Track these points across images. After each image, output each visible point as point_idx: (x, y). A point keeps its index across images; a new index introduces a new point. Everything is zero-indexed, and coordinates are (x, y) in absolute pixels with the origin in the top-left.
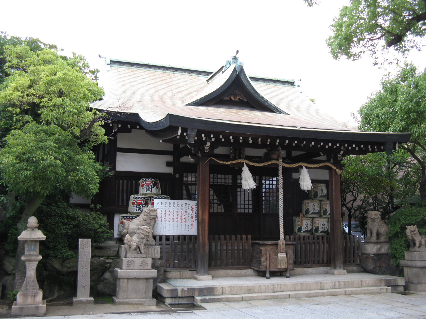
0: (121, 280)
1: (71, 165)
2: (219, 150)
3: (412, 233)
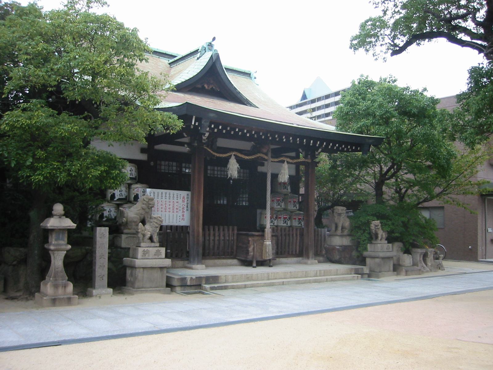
0: (138, 270)
3: (376, 227)
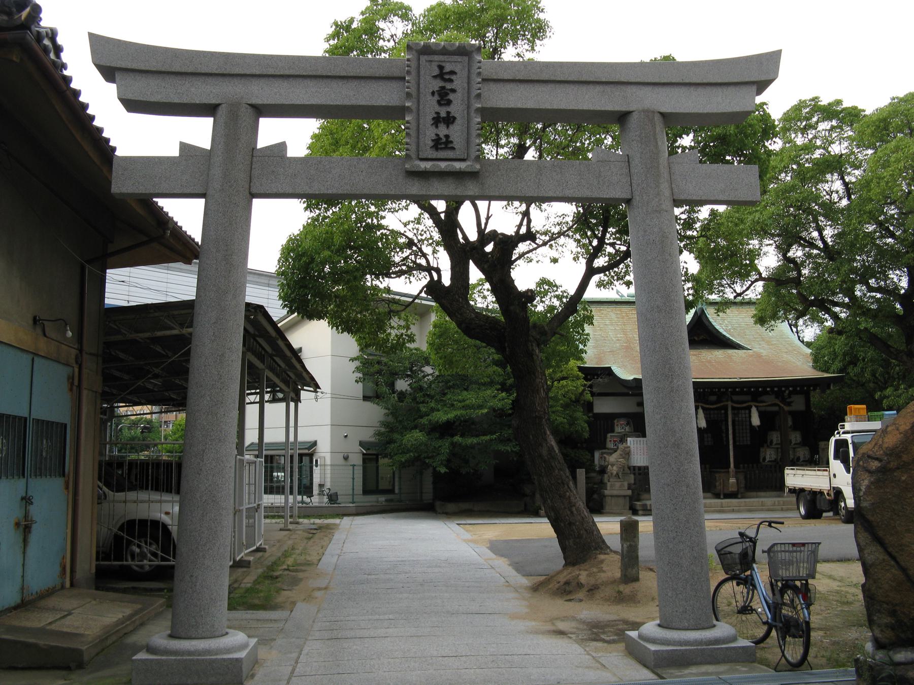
1: (572, 421)
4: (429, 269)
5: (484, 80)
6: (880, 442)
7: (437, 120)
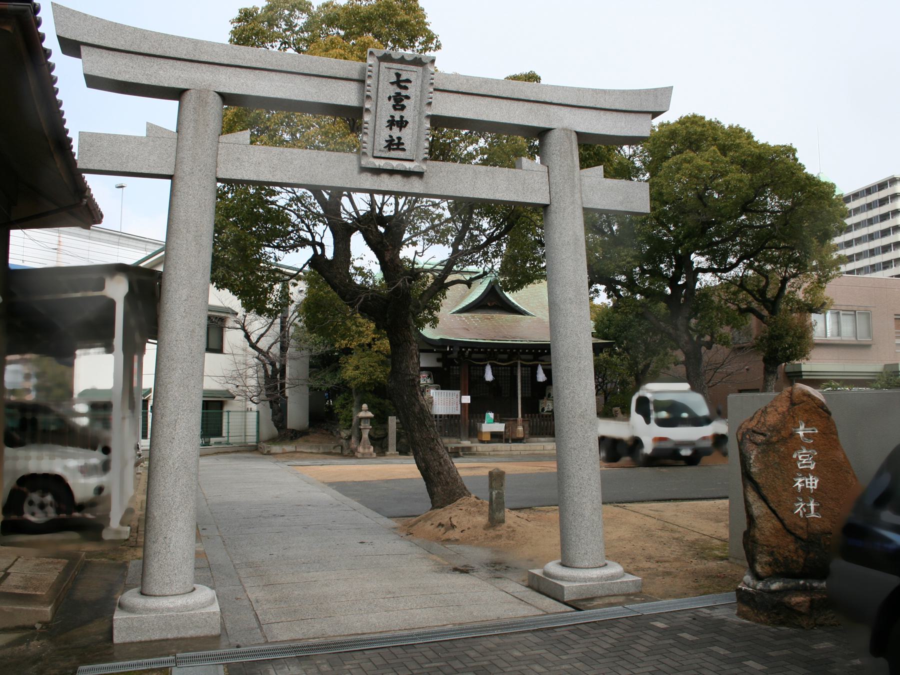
2: (474, 356)
4: (313, 244)
5: (435, 90)
6: (762, 420)
7: (392, 123)
